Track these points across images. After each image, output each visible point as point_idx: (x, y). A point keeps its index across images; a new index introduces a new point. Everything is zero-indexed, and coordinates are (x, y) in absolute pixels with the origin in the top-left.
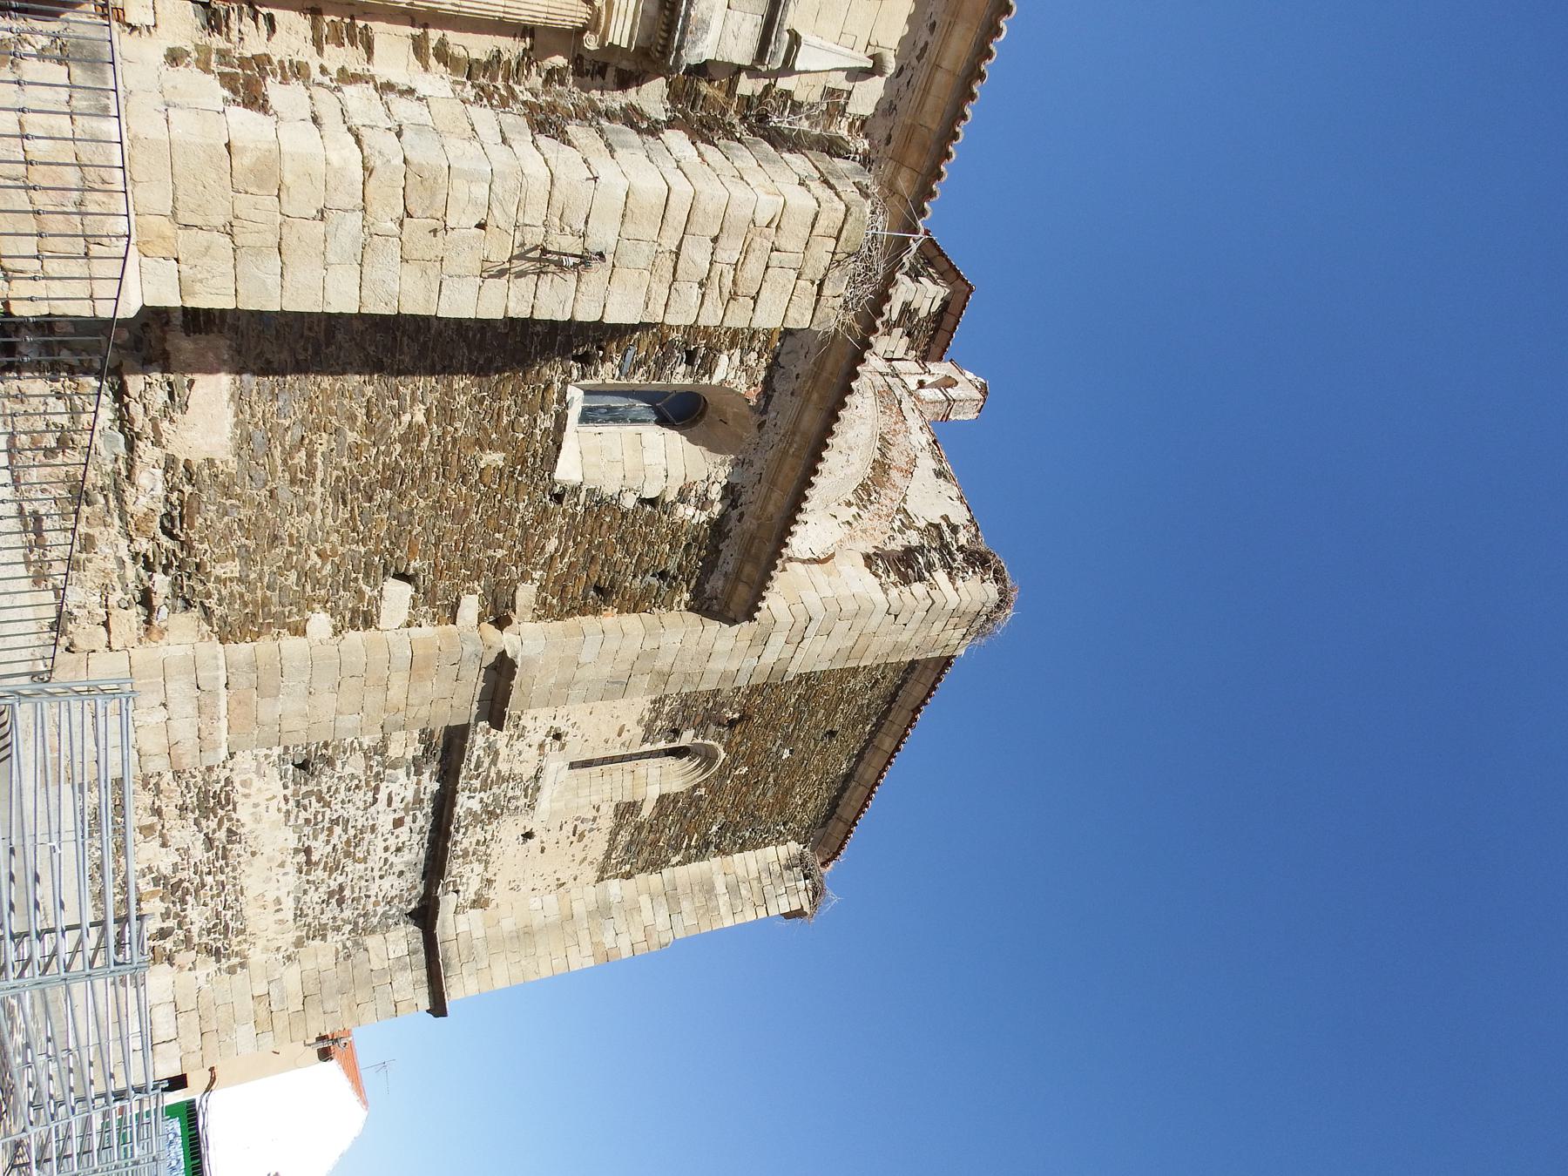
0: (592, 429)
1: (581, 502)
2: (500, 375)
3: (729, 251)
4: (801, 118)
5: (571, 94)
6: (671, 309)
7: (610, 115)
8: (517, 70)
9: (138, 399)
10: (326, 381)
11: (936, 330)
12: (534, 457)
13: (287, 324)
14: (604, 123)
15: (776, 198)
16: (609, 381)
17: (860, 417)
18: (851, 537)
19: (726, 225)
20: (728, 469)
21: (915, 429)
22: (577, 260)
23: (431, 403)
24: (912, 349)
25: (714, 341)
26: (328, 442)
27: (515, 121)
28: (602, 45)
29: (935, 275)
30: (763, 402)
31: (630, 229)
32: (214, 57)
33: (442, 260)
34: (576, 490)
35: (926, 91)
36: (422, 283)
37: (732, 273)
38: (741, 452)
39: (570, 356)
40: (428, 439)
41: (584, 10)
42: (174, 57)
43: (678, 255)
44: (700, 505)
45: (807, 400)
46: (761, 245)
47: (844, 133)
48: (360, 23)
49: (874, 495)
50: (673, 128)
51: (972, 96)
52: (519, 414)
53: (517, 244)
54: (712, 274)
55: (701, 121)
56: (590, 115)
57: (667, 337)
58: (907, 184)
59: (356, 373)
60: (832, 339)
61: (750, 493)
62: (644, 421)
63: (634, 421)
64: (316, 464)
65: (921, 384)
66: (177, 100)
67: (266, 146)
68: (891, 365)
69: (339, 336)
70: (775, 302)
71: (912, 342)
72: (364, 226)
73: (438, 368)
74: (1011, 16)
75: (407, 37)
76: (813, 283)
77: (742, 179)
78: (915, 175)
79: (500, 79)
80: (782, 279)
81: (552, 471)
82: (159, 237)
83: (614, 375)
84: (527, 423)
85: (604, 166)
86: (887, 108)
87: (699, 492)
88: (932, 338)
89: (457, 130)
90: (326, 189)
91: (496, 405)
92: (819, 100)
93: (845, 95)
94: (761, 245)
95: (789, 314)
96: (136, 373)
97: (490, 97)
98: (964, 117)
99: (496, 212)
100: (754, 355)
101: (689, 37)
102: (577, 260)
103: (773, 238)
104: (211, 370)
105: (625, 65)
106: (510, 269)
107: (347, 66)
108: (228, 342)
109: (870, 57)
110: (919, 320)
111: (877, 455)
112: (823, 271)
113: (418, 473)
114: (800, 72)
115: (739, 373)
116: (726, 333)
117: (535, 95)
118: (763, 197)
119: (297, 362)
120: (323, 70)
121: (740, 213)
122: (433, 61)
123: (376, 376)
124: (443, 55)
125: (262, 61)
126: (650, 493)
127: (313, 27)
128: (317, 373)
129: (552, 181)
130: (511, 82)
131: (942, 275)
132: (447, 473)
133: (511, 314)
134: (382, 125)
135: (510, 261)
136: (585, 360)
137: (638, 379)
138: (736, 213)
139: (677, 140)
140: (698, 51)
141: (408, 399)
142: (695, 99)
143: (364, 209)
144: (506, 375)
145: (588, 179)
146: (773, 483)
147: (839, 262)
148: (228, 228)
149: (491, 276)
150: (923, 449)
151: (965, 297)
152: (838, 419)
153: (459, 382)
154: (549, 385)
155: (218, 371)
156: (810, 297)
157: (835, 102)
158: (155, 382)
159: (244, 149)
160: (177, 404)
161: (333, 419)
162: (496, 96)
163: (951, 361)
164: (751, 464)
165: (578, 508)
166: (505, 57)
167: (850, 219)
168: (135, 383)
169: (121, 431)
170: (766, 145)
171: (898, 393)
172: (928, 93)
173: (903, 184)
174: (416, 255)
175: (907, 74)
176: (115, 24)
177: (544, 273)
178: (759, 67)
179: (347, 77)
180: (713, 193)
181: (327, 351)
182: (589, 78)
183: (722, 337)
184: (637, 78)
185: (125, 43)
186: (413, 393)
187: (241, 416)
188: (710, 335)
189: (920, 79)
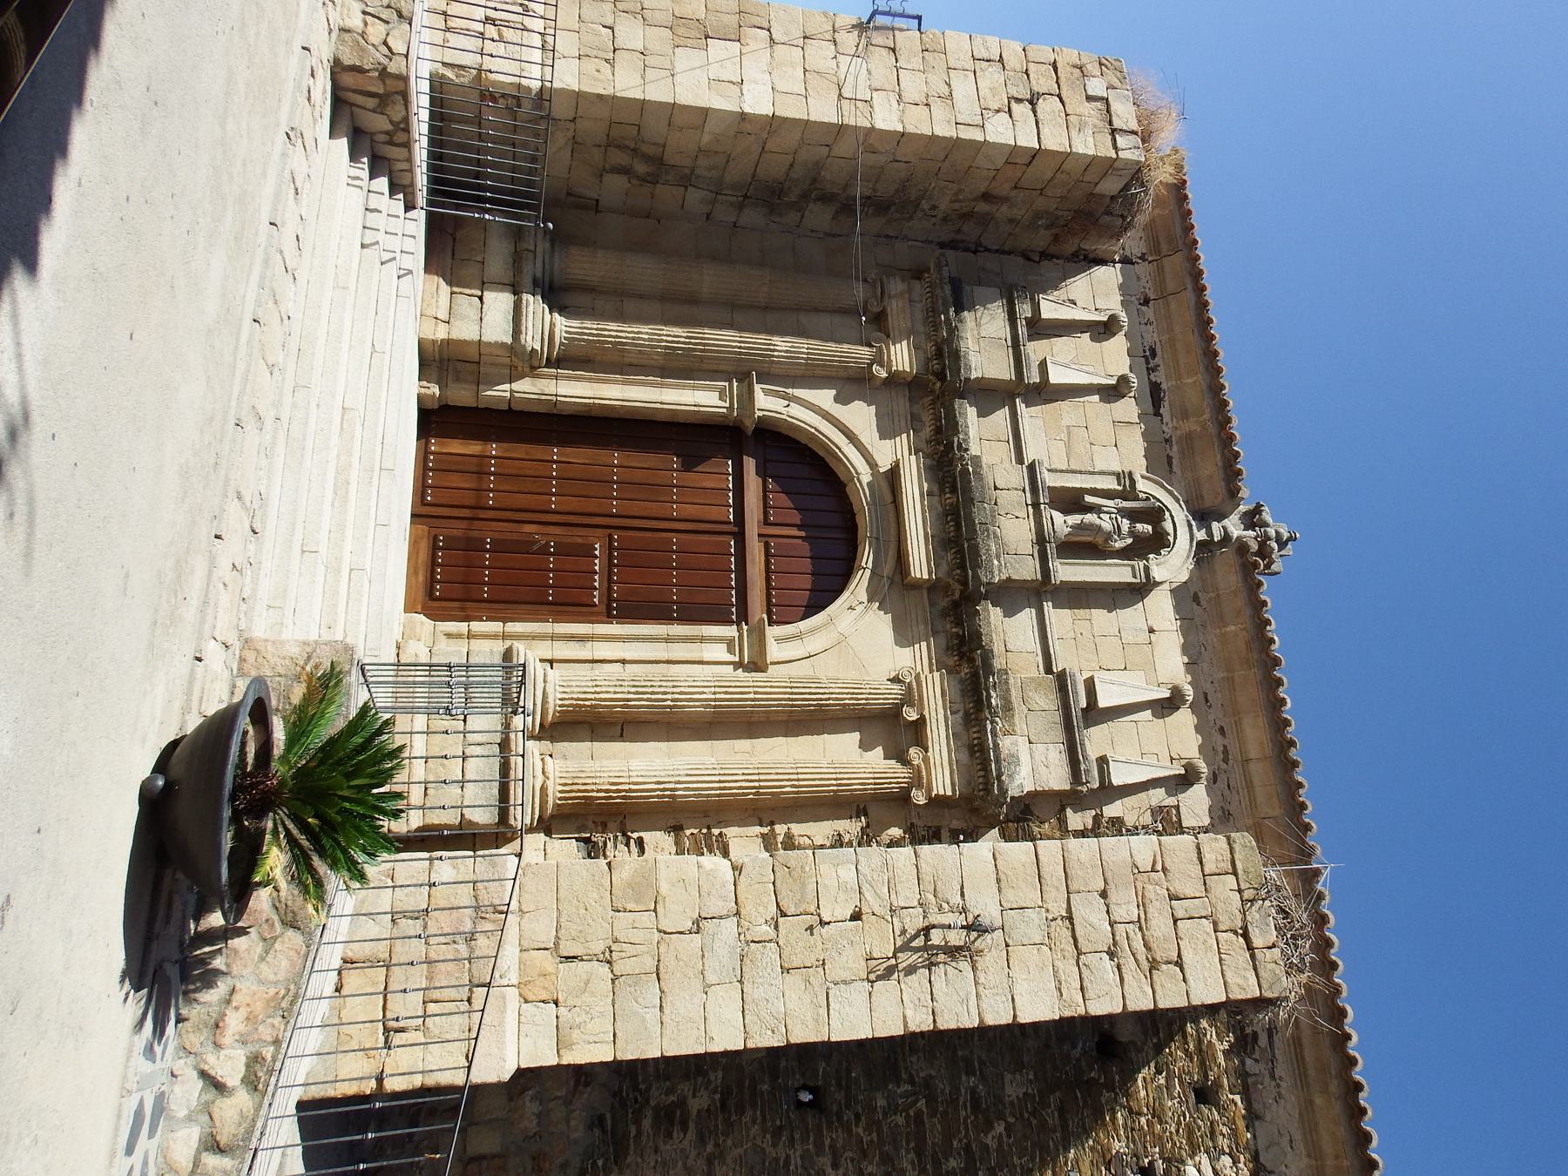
6: (1090, 994)
19: (1109, 875)
33: (824, 964)
35: (1250, 786)
36: (807, 998)
43: (1070, 918)
46: (1157, 893)
48: (716, 832)
53: (898, 932)
54: (1117, 938)
57: (1109, 1151)
70: (1204, 966)
72: (739, 934)
74: (1286, 686)
75: (757, 836)
76: (1235, 933)
82: (539, 975)
90: (700, 896)
94: (1157, 893)
98: (1300, 785)
99: (867, 895)
112: (1239, 916)
116: (1178, 1131)
127: (676, 844)
135: (894, 956)
140: (1017, 782)
143: (738, 913)
148: (607, 954)
149: (879, 978)
156: (1242, 952)
172: (1301, 1045)
175: (1222, 778)
178: (1079, 788)
183: (1175, 1138)
188: (1160, 1138)
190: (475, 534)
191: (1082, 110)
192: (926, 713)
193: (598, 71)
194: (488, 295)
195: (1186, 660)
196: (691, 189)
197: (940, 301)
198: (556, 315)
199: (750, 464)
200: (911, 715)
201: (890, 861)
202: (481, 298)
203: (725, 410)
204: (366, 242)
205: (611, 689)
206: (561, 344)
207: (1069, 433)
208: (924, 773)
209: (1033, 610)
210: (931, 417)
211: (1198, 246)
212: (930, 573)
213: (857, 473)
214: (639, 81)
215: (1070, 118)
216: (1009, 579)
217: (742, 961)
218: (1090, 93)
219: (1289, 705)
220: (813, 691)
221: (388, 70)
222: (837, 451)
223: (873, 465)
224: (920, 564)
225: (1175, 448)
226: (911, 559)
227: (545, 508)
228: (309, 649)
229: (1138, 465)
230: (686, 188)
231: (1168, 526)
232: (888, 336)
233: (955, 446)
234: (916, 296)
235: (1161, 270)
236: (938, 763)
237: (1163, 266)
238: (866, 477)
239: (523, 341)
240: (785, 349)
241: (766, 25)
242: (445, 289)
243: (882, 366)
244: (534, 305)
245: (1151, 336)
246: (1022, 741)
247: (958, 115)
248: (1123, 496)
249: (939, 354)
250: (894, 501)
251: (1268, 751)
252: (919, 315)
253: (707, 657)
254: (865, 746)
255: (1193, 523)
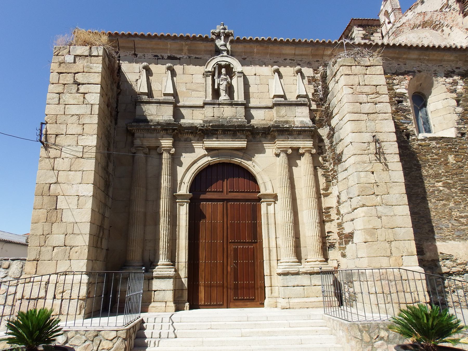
0: (433, 128)
1: (463, 126)
2: (419, 161)
3: (363, 98)
4: (318, 89)
5: (328, 154)
6: (386, 111)
7: (331, 142)
8: (325, 169)
9: (450, 269)
10: (433, 214)
11: (368, 26)
12: (448, 145)
13: (415, 226)
14: (334, 143)
15: (344, 89)
16: (414, 126)
17: (406, 39)
18: (457, 25)
19: (355, 101)
20: (439, 78)
21: (407, 18)
22: (377, 143)
23: (434, 181)
24: (377, 31)
25: (392, 95)
26: (455, 212)
27: (340, 168)
28: (314, 148)
29: (351, 33)
30: (411, 73)
31: (364, 130)
32: (341, 246)
33: (386, 183)
34: (458, 129)
35: (302, 55)
37: (370, 95)
38: (431, 75)
39: (408, 140)
40: (448, 181)
41: (306, 154)
42: (344, 256)
43: (368, 114)
44: (456, 84)
45: (407, 59)
46: (359, 89)
47: (319, 75)
48: (324, 211)
49: (437, 23)
50: (331, 124)
51: (300, 41)
52: (433, 153)
53: (376, 162)
54: (372, 102)
55: (327, 117)
56: (333, 148)
57: (395, 111)
58: (329, 51)
59: (428, 205)
60: (385, 58)
61: (447, 68)
62: (426, 112)
63: (427, 115)
64: (465, 215)
65: (389, 23)
66: (355, 255)
67: (363, 233)
68: (385, 36)
69: (416, 210)
71: (374, 32)
72: (381, 206)
73: (421, 180)
74: (277, 38)
76: (367, 69)
77: (340, 100)
78: (325, 49)
79: (329, 174)
80: (368, 80)
81: (452, 138)
82: (396, 261)
83: (412, 125)
84: (435, 150)
85: (347, 140)
86: (309, 65)
87: (450, 86)
88: (371, 26)
89: (346, 183)
91: (431, 161)
92: (312, 85)
93: (309, 78)
94: (359, 89)
95: (379, 73)
96: (441, 269)
97: (335, 175)
98: (306, 41)
100: (394, 81)
101: (306, 125)
102: (377, 143)
103: (356, 86)
104: (436, 248)
105: (317, 141)
106: (384, 163)
107: (335, 213)
108: (425, 243)
109: (297, 74)
110: (366, 32)
111: (420, 27)
112: (362, 67)
113: (462, 183)
114: (306, 93)
115: (402, 84)
117: (331, 163)
118: (344, 92)
119: (427, 222)
120: (338, 219)
121: (351, 98)
122: (329, 191)
123: (428, 199)
124: (327, 189)
125: (340, 234)
126: (455, 103)
127: (328, 222)
128: (430, 216)
129: (355, 155)
130: (329, 171)
131: (350, 31)
132: (460, 173)
133: (399, 160)
134: (350, 203)
135: (382, 163)
136: (408, 135)
137: (411, 117)
138: (351, 99)
139: (334, 122)
140: (308, 122)
141: (434, 188)
142: (321, 120)
143: (375, 206)
144: (419, 159)
145: (352, 145)
146: (441, 61)
147: (358, 63)
148: (389, 242)
149: (388, 168)
150: (414, 12)
151: (355, 20)
152: (411, 46)
153: (424, 173)
154: (420, 145)
155: (436, 246)
157: (312, 80)
158: (443, 264)
159: (365, 238)
160: (450, 258)
161: (446, 211)
162: (334, 174)
163: (378, 16)
164: (435, 71)
165: (466, 127)
166: (323, 173)
167: (344, 64)
168: (444, 270)
169: (463, 274)
170: (329, 96)
171: (394, 30)
173: (329, 52)
174: (386, 190)
176: (338, 269)
177: (383, 152)
179: (338, 213)
180: (347, 108)
181: (422, 214)
182: (323, 150)
183: (390, 93)
184: (320, 137)
185: (343, 267)
186: (431, 187)
187: (451, 239)
189: (299, 58)
190: (232, 287)
191: (81, 66)
192: (289, 146)
193: (76, 252)
194: (154, 288)
195: (264, 66)
196: (105, 216)
197: (146, 127)
198: (159, 263)
199: (202, 197)
200: (290, 151)
201: (358, 162)
202: (155, 291)
203: (188, 204)
204: (174, 336)
205: (289, 242)
206: (168, 261)
207: (189, 89)
208: (282, 149)
209: (251, 110)
210: (187, 135)
211: (118, 32)
212: (245, 141)
213: (208, 161)
214: (80, 236)
215: (85, 70)
216: (245, 116)
217: (387, 205)
218: (73, 61)
219: (283, 39)
220: (285, 180)
221: (125, 337)
222: (200, 167)
223: (205, 156)
224: (242, 144)
225: (192, 55)
226: (240, 146)
227: (222, 264)
228: (353, 338)
229: (202, 69)
230: (105, 217)
231: (223, 63)
232: (159, 147)
233: (202, 128)
234: (142, 135)
235: (123, 47)
236: (304, 145)
237: (122, 46)
238: (209, 159)
239: (173, 275)
240: (166, 183)
241: (48, 185)
242: (152, 304)
243: (171, 150)
244: (157, 272)
245: (149, 55)
246: (296, 119)
247: (87, 113)
248: (213, 76)
249: (166, 130)
250: (218, 150)
251: (294, 48)
252: (149, 135)
253: (273, 212)
254: (296, 166)
255: (221, 55)
